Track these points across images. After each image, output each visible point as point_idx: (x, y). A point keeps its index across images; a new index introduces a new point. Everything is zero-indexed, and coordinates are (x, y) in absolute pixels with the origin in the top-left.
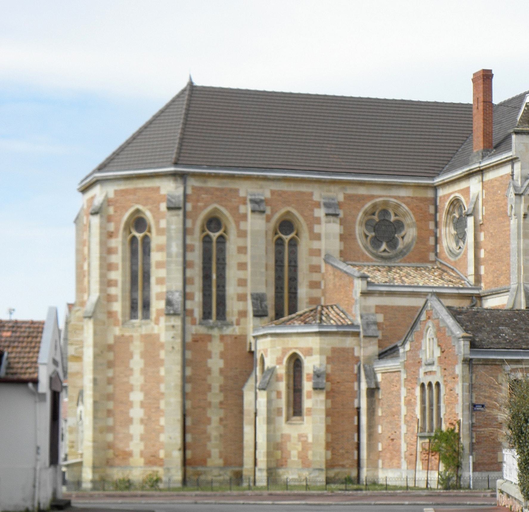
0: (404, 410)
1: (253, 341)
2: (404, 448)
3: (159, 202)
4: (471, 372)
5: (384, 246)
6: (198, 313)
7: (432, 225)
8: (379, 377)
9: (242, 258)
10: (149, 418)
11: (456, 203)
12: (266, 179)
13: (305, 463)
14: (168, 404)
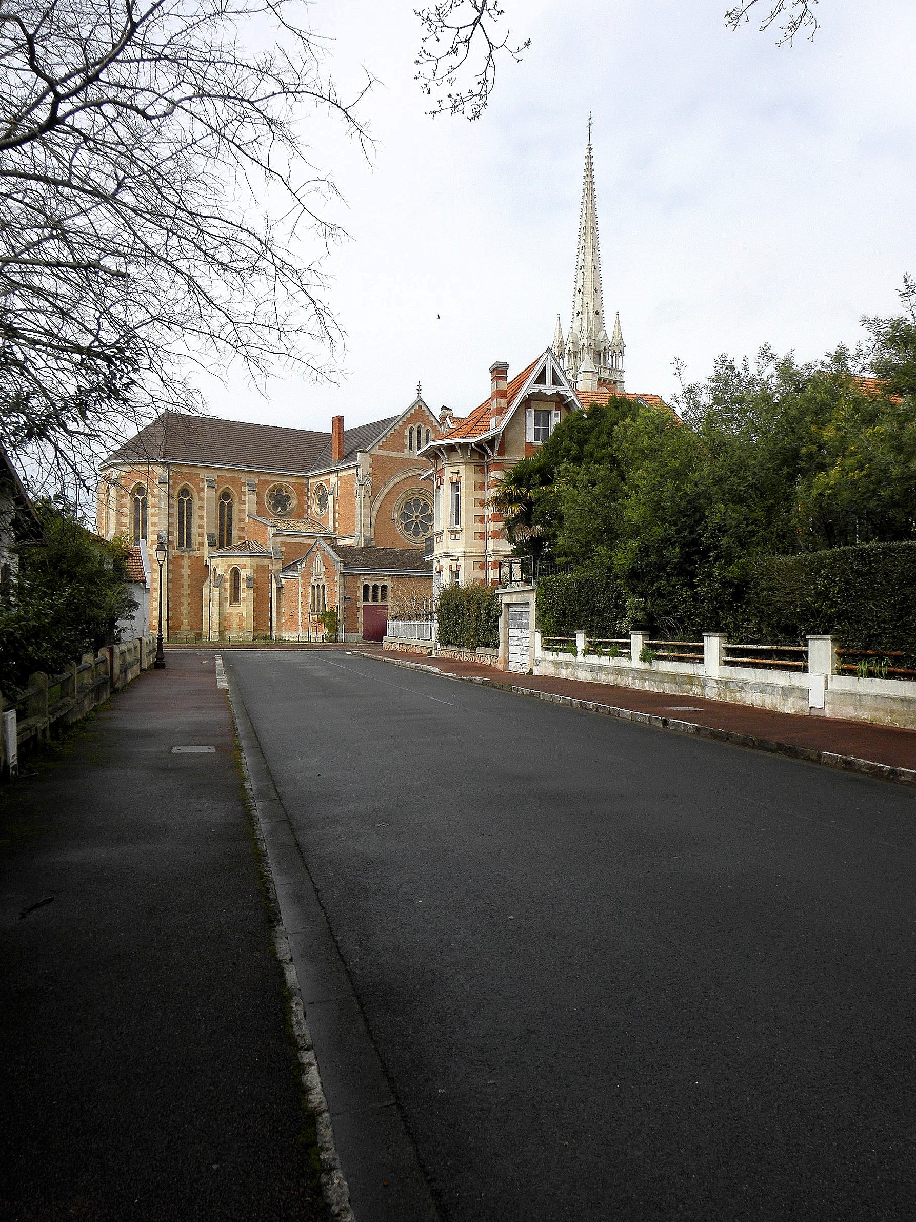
0: (301, 600)
1: (208, 559)
2: (300, 619)
4: (344, 580)
6: (176, 543)
8: (283, 581)
9: (201, 513)
11: (321, 487)
12: (215, 468)
13: (241, 628)
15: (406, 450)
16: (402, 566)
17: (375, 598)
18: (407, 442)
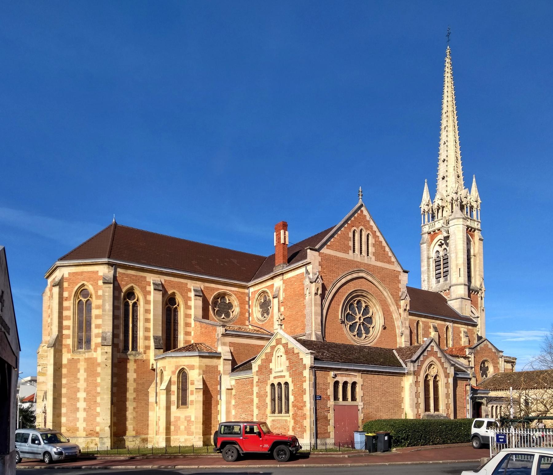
0: (256, 400)
1: (154, 362)
3: (98, 280)
5: (223, 316)
7: (247, 307)
10: (90, 408)
14: (102, 399)
15: (351, 252)
16: (368, 362)
17: (345, 398)
18: (351, 244)
